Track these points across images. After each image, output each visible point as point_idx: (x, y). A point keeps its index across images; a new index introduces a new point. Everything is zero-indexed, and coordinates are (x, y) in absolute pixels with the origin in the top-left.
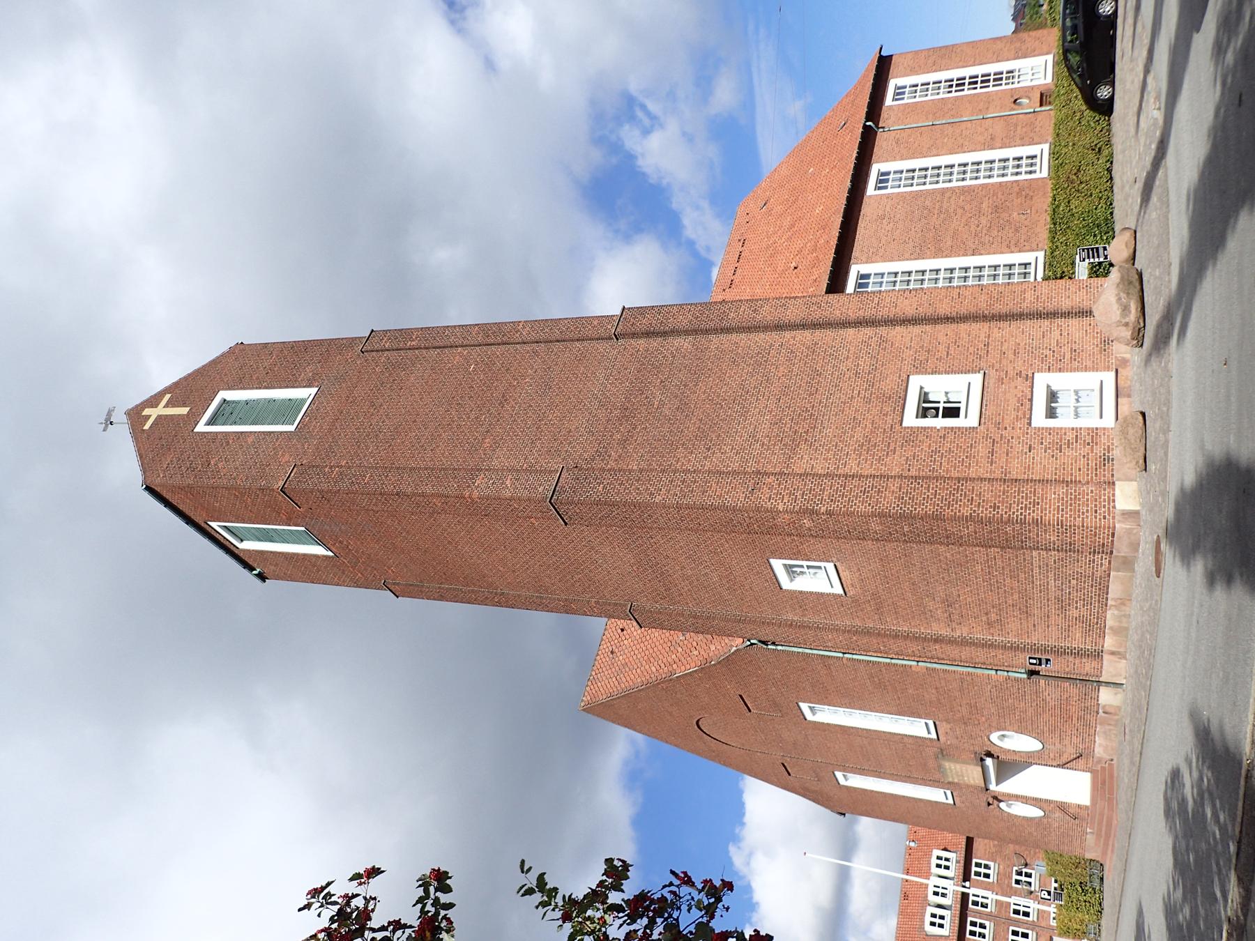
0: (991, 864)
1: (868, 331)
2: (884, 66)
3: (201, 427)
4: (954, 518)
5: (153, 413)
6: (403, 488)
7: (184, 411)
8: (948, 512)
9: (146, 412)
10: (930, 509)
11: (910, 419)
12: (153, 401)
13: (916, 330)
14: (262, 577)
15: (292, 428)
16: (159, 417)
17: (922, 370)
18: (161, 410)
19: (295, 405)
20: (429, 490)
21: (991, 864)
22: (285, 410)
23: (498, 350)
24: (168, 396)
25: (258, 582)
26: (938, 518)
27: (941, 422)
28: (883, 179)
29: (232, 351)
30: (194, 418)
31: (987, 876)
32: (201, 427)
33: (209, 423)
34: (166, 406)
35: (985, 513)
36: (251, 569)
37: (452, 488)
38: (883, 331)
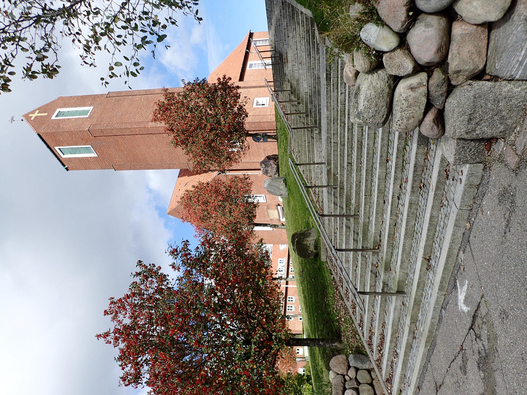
0: (293, 297)
1: (246, 89)
2: (251, 35)
3: (53, 118)
4: (263, 122)
5: (34, 116)
6: (128, 127)
7: (46, 114)
8: (262, 121)
9: (30, 115)
10: (258, 121)
11: (255, 106)
12: (33, 112)
13: (256, 89)
14: (67, 169)
15: (87, 116)
16: (36, 117)
17: (257, 97)
18: (36, 114)
19: (88, 111)
20: (135, 127)
21: (293, 297)
22: (86, 112)
23: (150, 96)
24: (37, 111)
25: (66, 170)
26: (260, 122)
27: (261, 106)
28: (251, 66)
29: (59, 99)
30: (50, 116)
31: (292, 301)
32: (53, 118)
33: (56, 117)
34: (38, 113)
35: (269, 120)
36: (64, 166)
37: (142, 126)
38: (249, 89)
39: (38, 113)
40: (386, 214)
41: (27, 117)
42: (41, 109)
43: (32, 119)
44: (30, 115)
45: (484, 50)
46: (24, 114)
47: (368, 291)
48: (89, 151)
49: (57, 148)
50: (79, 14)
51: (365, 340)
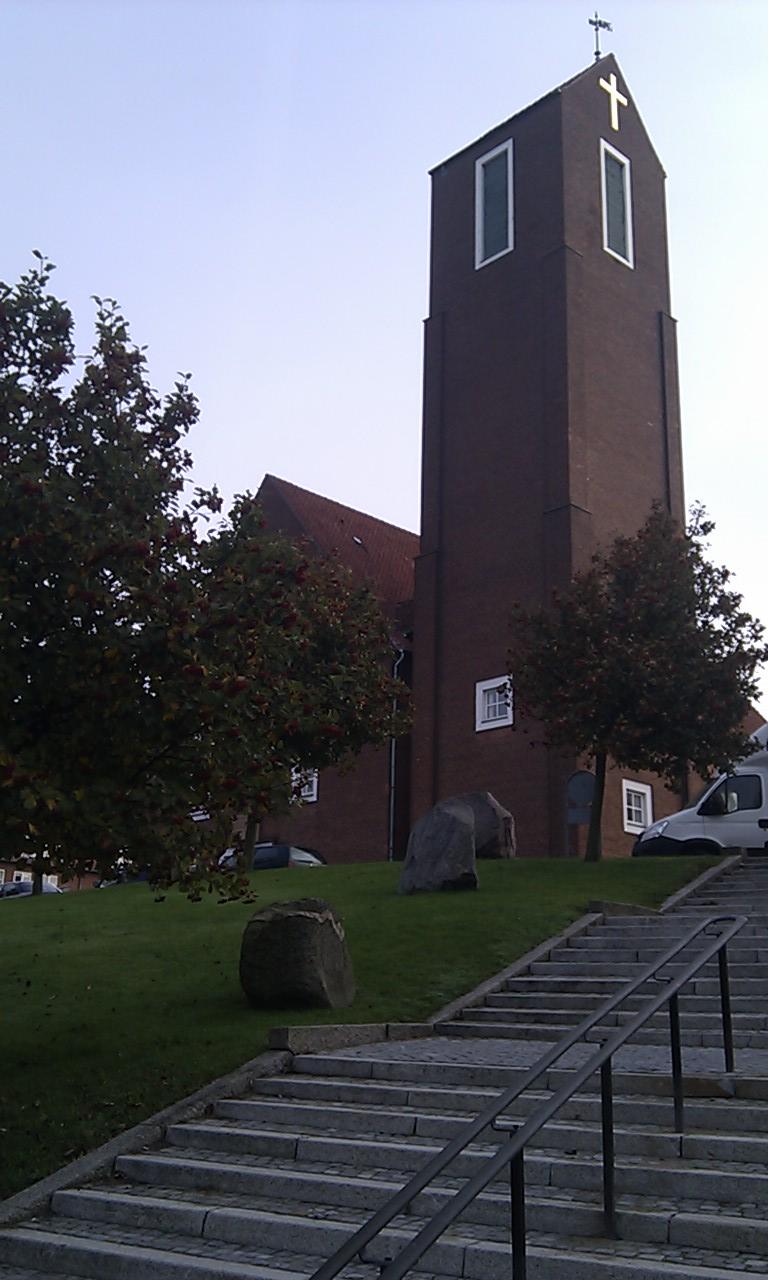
3: (604, 145)
5: (610, 87)
7: (615, 125)
9: (613, 78)
12: (622, 88)
18: (616, 97)
24: (624, 101)
29: (664, 173)
32: (604, 145)
34: (619, 104)
39: (619, 104)
40: (326, 1080)
41: (607, 66)
42: (629, 112)
43: (603, 82)
44: (613, 78)
45: (495, 1238)
46: (617, 58)
47: (529, 1251)
48: (494, 242)
49: (508, 145)
50: (301, 570)
51: (115, 1150)
